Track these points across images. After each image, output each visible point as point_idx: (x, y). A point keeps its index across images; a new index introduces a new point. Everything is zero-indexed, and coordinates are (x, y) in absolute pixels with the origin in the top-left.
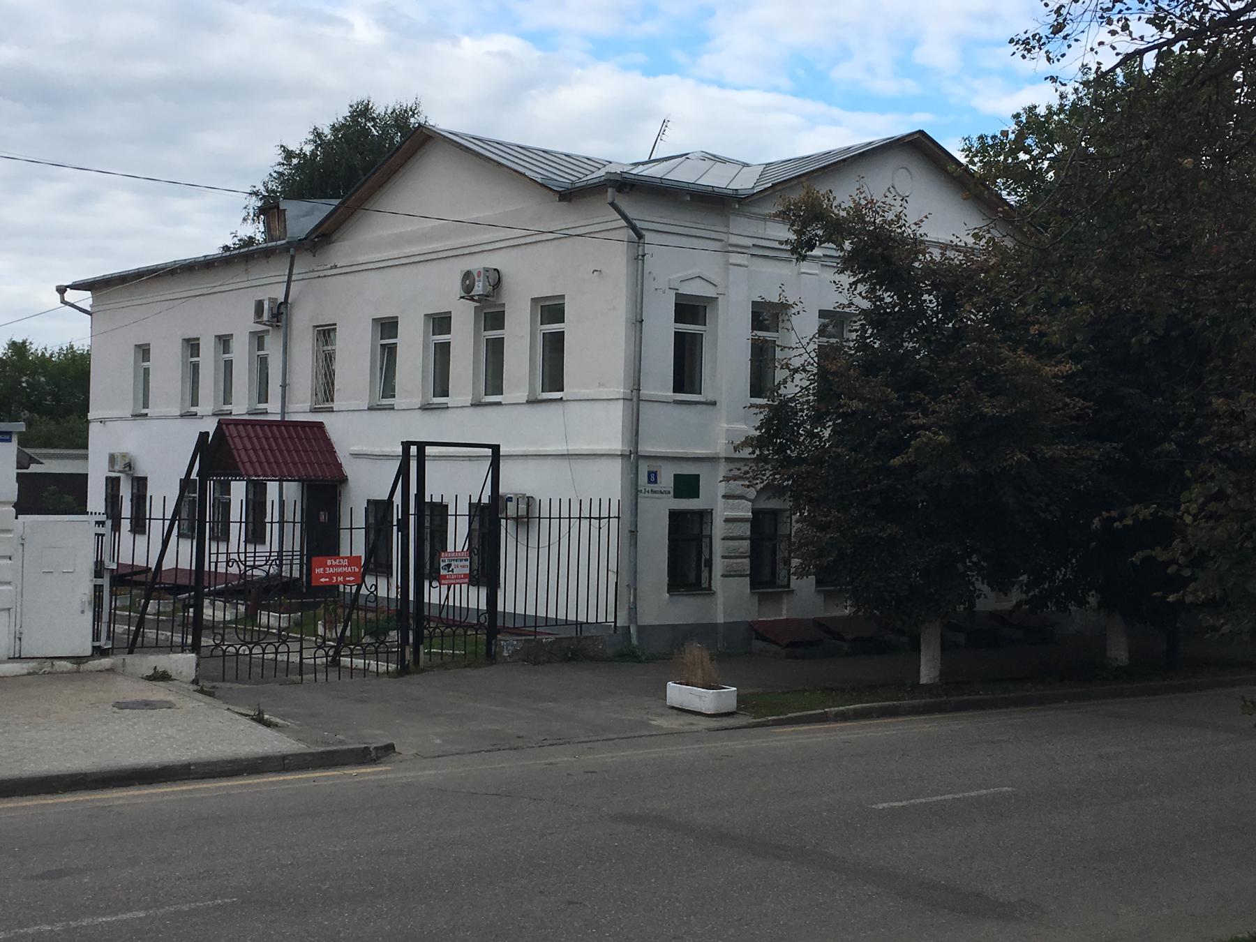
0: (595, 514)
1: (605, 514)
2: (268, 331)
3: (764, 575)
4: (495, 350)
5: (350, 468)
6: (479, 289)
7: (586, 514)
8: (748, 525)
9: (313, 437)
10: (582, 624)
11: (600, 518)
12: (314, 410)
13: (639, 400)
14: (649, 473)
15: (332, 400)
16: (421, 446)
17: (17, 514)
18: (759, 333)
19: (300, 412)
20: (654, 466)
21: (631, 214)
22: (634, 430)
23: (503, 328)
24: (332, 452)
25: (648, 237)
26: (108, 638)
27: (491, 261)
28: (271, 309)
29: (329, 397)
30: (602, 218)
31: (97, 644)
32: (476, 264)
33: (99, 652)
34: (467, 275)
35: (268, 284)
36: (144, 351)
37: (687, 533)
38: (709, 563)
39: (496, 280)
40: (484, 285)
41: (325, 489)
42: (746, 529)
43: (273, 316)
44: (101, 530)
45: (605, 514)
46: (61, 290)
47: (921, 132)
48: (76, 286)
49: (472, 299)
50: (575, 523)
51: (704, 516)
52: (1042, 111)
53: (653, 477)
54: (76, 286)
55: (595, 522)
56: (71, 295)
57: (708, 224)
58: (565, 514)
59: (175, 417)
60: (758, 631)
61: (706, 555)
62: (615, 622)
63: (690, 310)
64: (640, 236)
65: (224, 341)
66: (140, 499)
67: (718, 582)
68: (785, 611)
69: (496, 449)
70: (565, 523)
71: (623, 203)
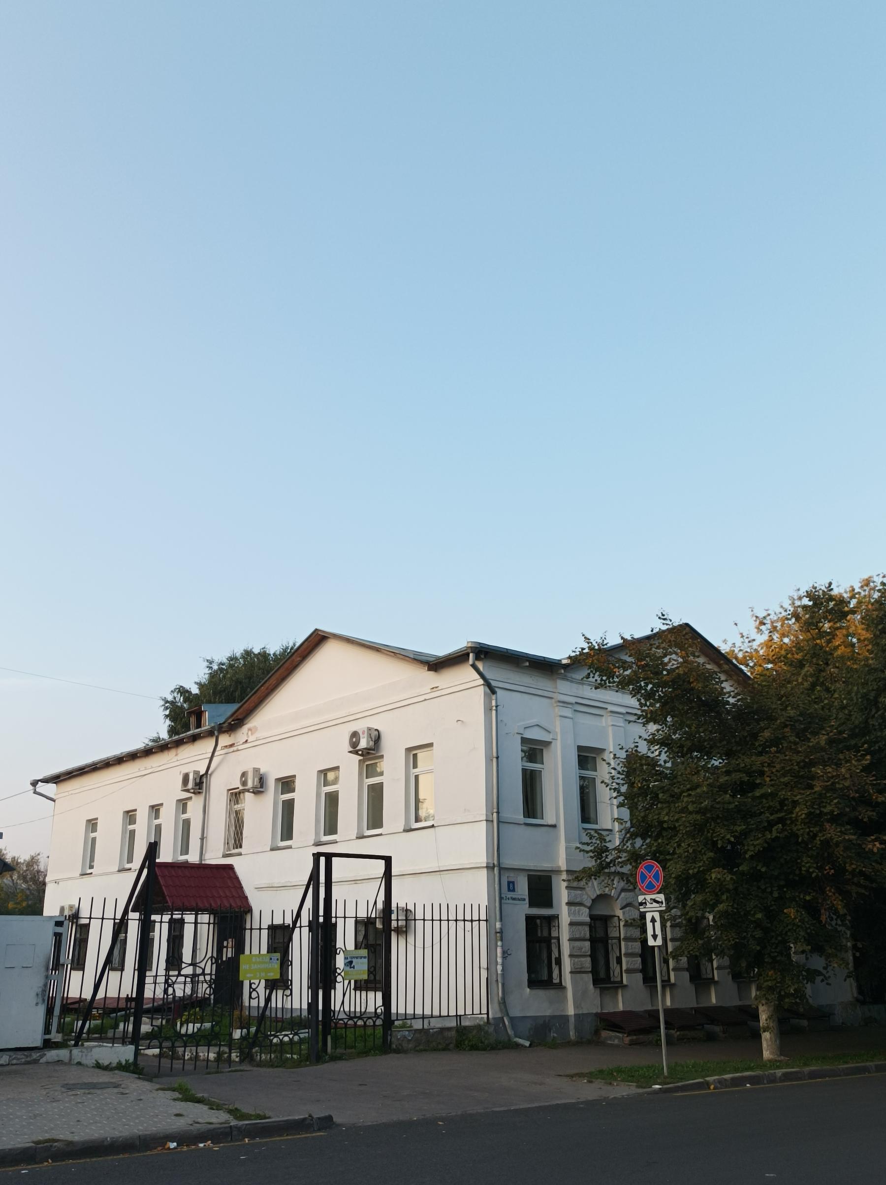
0: (468, 917)
1: (475, 917)
2: (190, 798)
4: (376, 795)
9: (225, 875)
10: (460, 1016)
11: (472, 921)
13: (499, 822)
14: (509, 883)
15: (241, 847)
16: (329, 857)
18: (583, 772)
19: (214, 857)
20: (512, 876)
25: (499, 691)
27: (375, 723)
28: (195, 779)
29: (238, 844)
30: (466, 676)
31: (47, 1037)
32: (360, 726)
33: (48, 1044)
34: (355, 734)
35: (193, 757)
36: (92, 824)
37: (539, 936)
38: (559, 962)
39: (377, 739)
40: (368, 743)
41: (232, 917)
42: (586, 932)
45: (475, 917)
46: (34, 783)
48: (46, 781)
49: (356, 753)
50: (428, 924)
51: (552, 920)
54: (46, 781)
56: (41, 787)
57: (541, 683)
59: (112, 873)
61: (555, 954)
62: (488, 1014)
64: (493, 692)
65: (155, 810)
66: (82, 943)
69: (388, 860)
70: (444, 924)
71: (480, 665)
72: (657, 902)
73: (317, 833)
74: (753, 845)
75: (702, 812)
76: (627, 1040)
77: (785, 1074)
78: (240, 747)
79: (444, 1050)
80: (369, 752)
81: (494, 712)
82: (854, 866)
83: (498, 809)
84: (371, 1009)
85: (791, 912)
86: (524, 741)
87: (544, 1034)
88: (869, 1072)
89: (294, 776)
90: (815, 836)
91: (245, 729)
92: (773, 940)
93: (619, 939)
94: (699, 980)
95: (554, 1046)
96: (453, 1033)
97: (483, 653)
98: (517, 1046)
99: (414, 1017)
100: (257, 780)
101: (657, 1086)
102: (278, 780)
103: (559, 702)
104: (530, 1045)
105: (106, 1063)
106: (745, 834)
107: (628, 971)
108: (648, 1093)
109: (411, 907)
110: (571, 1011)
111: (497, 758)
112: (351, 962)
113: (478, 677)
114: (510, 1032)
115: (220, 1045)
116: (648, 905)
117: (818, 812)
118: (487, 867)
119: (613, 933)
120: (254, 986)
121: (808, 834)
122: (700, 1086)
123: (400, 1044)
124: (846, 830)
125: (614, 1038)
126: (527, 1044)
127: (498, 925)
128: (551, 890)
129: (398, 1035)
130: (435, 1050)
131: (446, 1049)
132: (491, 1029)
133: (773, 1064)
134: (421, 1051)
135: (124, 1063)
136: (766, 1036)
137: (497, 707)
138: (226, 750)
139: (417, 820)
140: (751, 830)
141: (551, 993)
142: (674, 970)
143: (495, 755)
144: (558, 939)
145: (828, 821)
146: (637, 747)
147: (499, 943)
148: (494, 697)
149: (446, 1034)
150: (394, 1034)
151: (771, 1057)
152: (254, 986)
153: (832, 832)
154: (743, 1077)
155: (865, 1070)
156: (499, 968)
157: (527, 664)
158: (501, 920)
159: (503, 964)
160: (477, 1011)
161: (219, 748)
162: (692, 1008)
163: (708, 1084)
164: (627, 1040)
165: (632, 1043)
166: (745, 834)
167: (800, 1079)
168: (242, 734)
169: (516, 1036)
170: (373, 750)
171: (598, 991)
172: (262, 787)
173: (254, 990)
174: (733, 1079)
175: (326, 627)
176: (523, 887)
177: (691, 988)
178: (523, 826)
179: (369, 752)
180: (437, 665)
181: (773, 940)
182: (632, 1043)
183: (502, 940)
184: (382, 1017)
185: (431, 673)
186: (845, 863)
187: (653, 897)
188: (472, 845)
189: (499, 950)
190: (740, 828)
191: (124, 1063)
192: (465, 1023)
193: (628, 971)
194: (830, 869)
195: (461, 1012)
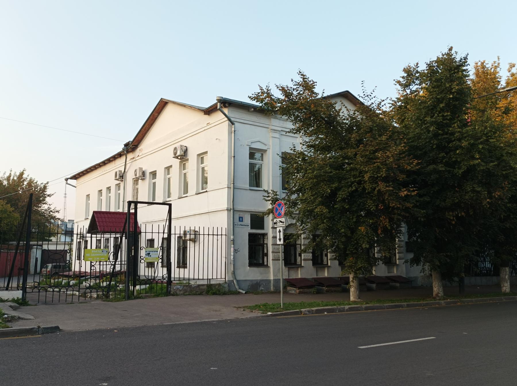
0: (215, 233)
1: (220, 233)
3: (290, 257)
11: (217, 235)
13: (234, 188)
14: (240, 218)
16: (136, 203)
20: (242, 214)
22: (233, 200)
25: (236, 124)
27: (184, 143)
32: (177, 145)
34: (175, 149)
38: (267, 255)
40: (180, 152)
43: (120, 177)
46: (67, 180)
47: (347, 91)
48: (72, 178)
49: (177, 158)
50: (206, 237)
52: (415, 265)
53: (241, 219)
54: (72, 178)
55: (215, 237)
56: (70, 181)
60: (290, 283)
64: (233, 124)
65: (109, 189)
67: (271, 263)
68: (299, 274)
69: (170, 205)
71: (226, 111)
72: (282, 222)
73: (164, 197)
74: (341, 195)
75: (316, 177)
76: (298, 291)
77: (349, 308)
78: (137, 159)
79: (199, 294)
80: (183, 156)
81: (233, 134)
82: (394, 204)
83: (234, 182)
84: (160, 275)
85: (362, 229)
86: (251, 149)
87: (255, 288)
88: (403, 307)
89: (156, 171)
90: (375, 188)
91: (138, 149)
92: (352, 243)
93: (301, 245)
94: (318, 262)
95: (262, 293)
96: (205, 287)
97: (226, 103)
98: (239, 293)
99: (184, 279)
100: (141, 173)
101: (270, 313)
102: (151, 173)
103: (272, 130)
104: (245, 293)
105: (6, 299)
106: (338, 189)
107: (305, 260)
108: (265, 316)
109: (197, 229)
110: (272, 278)
111: (234, 157)
112: (149, 254)
113: (224, 116)
114: (237, 287)
115: (97, 292)
116: (278, 224)
117: (376, 176)
118: (227, 210)
119: (298, 242)
120: (92, 264)
121: (371, 188)
122: (296, 313)
123: (175, 292)
124: (390, 185)
125: (292, 290)
126: (244, 292)
127: (232, 237)
128: (264, 221)
129: (174, 288)
130: (195, 294)
131: (201, 294)
132: (226, 285)
133: (354, 302)
134: (187, 295)
135: (16, 299)
136: (352, 290)
137: (234, 131)
138: (131, 161)
139: (202, 189)
140: (342, 187)
141: (261, 269)
142: (330, 259)
143: (233, 155)
144: (267, 244)
145: (380, 180)
146: (295, 147)
147: (232, 246)
148: (233, 126)
149: (201, 287)
150: (172, 287)
151: (354, 299)
152: (92, 264)
153: (382, 186)
154: (323, 309)
155: (402, 306)
156: (232, 257)
157: (253, 109)
158: (233, 235)
159: (234, 256)
160: (219, 277)
161: (127, 160)
162: (339, 277)
163: (301, 312)
164: (298, 291)
165: (300, 293)
166: (338, 189)
167: (360, 310)
168: (138, 152)
169: (240, 289)
170: (184, 156)
171: (287, 268)
172: (144, 176)
173: (93, 266)
174: (317, 310)
175: (167, 97)
176: (247, 220)
177: (340, 268)
178: (249, 191)
179: (183, 156)
180: (209, 111)
181: (352, 243)
182: (300, 293)
183: (234, 244)
184: (167, 279)
185: (207, 116)
186: (389, 203)
187: (280, 219)
188: (219, 198)
189: (232, 249)
190: (335, 185)
191: (16, 299)
192: (212, 282)
193: (305, 260)
194: (382, 206)
195: (210, 277)
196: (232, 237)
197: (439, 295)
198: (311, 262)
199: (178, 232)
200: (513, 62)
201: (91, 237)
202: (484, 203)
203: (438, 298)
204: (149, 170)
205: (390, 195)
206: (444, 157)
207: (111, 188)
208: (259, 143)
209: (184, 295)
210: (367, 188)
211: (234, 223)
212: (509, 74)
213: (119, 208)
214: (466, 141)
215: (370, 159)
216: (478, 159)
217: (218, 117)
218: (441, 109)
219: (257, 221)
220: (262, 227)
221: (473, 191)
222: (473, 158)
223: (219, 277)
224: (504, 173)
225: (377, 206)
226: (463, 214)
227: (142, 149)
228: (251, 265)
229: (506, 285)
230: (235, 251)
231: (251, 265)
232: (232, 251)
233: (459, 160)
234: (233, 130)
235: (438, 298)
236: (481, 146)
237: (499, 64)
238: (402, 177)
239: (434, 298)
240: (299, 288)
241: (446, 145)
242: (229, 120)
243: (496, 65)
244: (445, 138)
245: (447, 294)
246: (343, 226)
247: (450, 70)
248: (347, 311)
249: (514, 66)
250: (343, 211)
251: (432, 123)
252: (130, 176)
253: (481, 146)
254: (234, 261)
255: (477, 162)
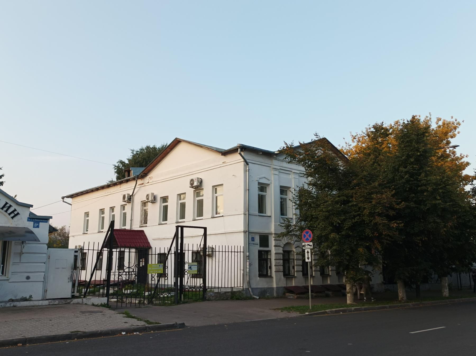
0: (236, 251)
5: (153, 244)
6: (195, 184)
7: (233, 250)
8: (282, 255)
12: (140, 227)
13: (249, 214)
14: (252, 238)
16: (182, 227)
17: (48, 248)
19: (136, 227)
21: (245, 158)
22: (248, 224)
23: (184, 218)
24: (146, 238)
25: (250, 164)
26: (77, 292)
27: (200, 176)
29: (146, 222)
33: (73, 297)
35: (127, 188)
36: (87, 214)
37: (263, 258)
38: (270, 268)
41: (143, 250)
42: (281, 256)
43: (128, 199)
44: (76, 254)
46: (63, 198)
48: (68, 197)
49: (193, 187)
51: (268, 252)
53: (253, 239)
54: (68, 197)
56: (66, 200)
57: (266, 161)
58: (227, 250)
59: (96, 233)
61: (269, 265)
63: (263, 187)
64: (248, 164)
65: (112, 209)
67: (274, 274)
68: (294, 283)
69: (205, 229)
71: (242, 153)
73: (177, 219)
74: (348, 224)
75: (328, 211)
80: (198, 187)
85: (361, 250)
86: (259, 183)
87: (264, 294)
90: (372, 221)
91: (148, 177)
94: (324, 275)
95: (268, 298)
96: (230, 293)
97: (244, 148)
98: (254, 298)
100: (153, 197)
102: (161, 198)
105: (96, 304)
106: (344, 220)
109: (214, 247)
110: (275, 286)
112: (191, 267)
113: (241, 158)
114: (251, 293)
119: (292, 257)
125: (291, 296)
126: (258, 298)
127: (248, 254)
128: (268, 241)
129: (208, 295)
130: (223, 300)
132: (244, 292)
133: (351, 305)
134: (217, 300)
139: (216, 214)
140: (347, 219)
141: (267, 279)
144: (270, 259)
145: (377, 215)
147: (248, 261)
153: (378, 219)
156: (248, 270)
158: (249, 252)
160: (239, 286)
161: (137, 185)
164: (296, 296)
165: (298, 298)
167: (361, 311)
168: (147, 179)
172: (155, 200)
173: (121, 275)
174: (336, 311)
178: (258, 217)
179: (198, 187)
180: (225, 153)
182: (298, 298)
185: (223, 156)
187: (308, 243)
188: (239, 223)
189: (248, 263)
190: (343, 218)
192: (234, 290)
195: (233, 286)
196: (248, 254)
197: (404, 299)
198: (301, 273)
199: (191, 248)
200: (440, 117)
201: (130, 252)
202: (442, 231)
203: (403, 301)
204: (160, 195)
205: (383, 226)
206: (413, 197)
207: (115, 209)
208: (264, 179)
209: (216, 300)
210: (366, 220)
211: (249, 242)
212: (436, 126)
213: (124, 225)
214: (430, 187)
215: (368, 199)
216: (439, 200)
217: (237, 158)
218: (411, 162)
219: (264, 240)
220: (268, 246)
221: (435, 222)
222: (435, 198)
223: (239, 286)
224: (455, 209)
225: (373, 233)
226: (426, 238)
227: (152, 177)
228: (260, 276)
229: (446, 290)
230: (250, 265)
231: (260, 276)
232: (248, 265)
233: (424, 199)
234: (248, 169)
235: (403, 301)
236: (441, 191)
237: (430, 119)
238: (392, 213)
239: (400, 301)
240: (296, 295)
241: (416, 188)
242: (245, 161)
243: (429, 119)
244: (415, 183)
245: (409, 298)
246: (347, 247)
247: (418, 135)
248: (354, 311)
249: (440, 120)
250: (348, 236)
251: (406, 173)
252: (138, 200)
253: (441, 191)
254: (249, 272)
255: (438, 202)
